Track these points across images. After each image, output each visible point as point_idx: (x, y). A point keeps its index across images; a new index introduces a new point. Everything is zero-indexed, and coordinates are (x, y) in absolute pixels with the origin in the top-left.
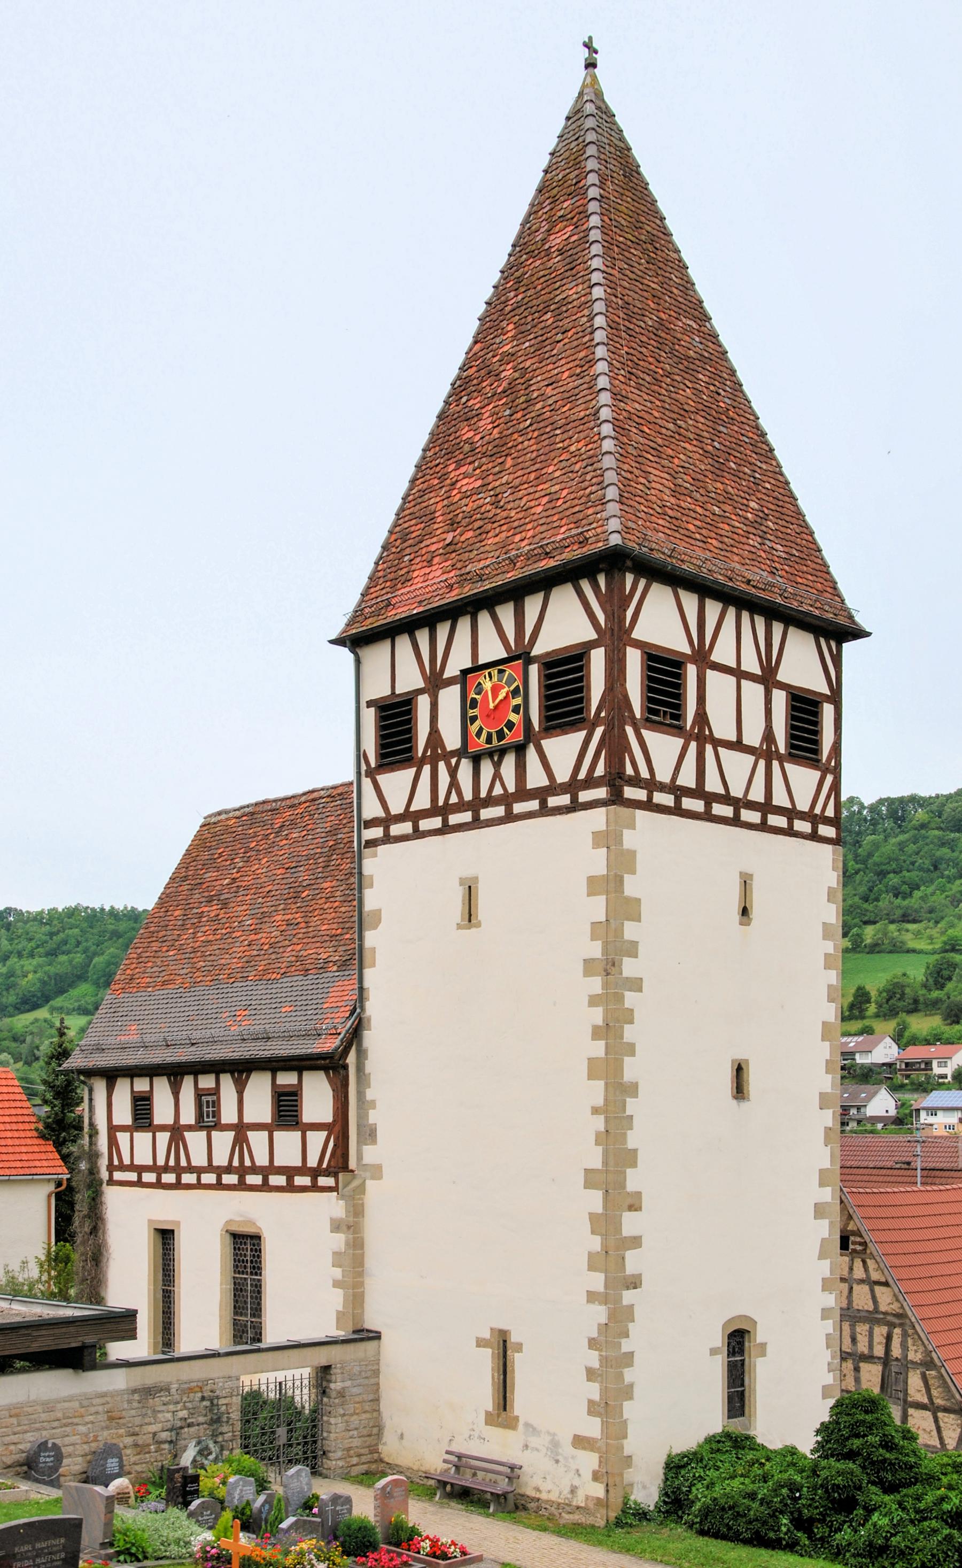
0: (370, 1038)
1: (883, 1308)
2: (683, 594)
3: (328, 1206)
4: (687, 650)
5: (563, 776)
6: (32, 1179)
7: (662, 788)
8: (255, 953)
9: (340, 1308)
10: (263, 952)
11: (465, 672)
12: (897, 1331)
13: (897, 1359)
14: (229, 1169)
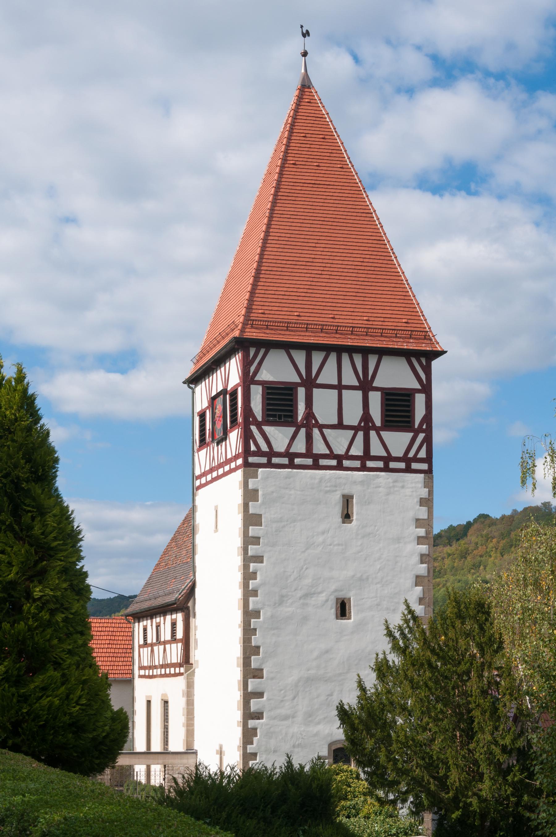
2: (294, 353)
4: (298, 380)
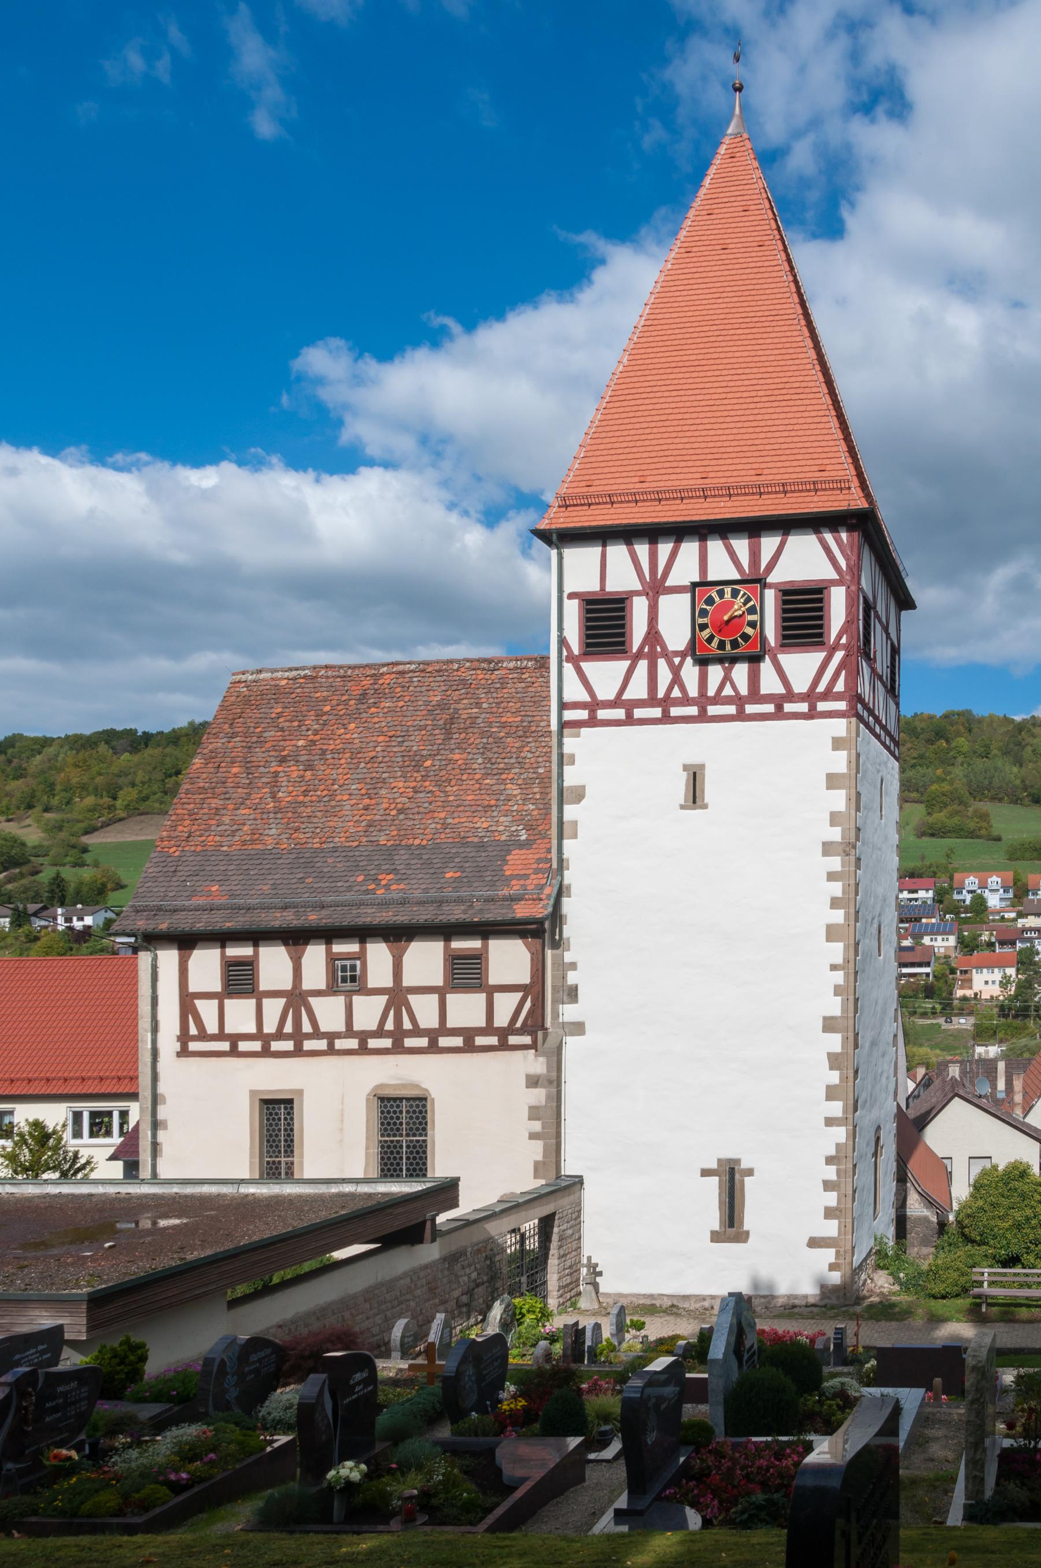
5: (800, 687)
9: (540, 1158)
11: (695, 585)
14: (279, 1035)
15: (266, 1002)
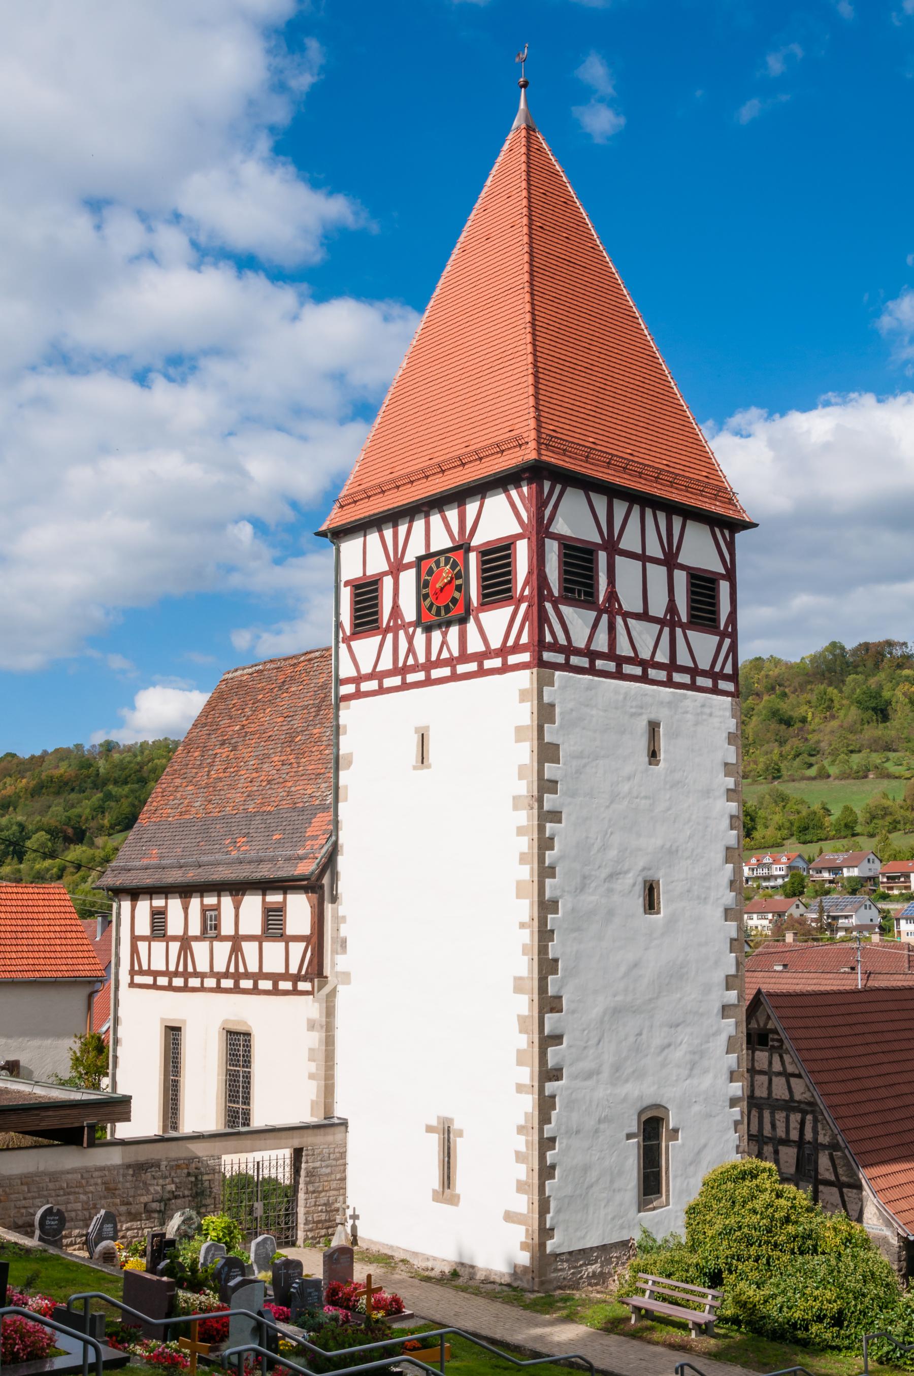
0: (342, 862)
1: (797, 1097)
3: (306, 1008)
5: (495, 644)
6: (76, 981)
7: (578, 652)
8: (255, 788)
10: (261, 788)
11: (420, 559)
12: (809, 1117)
13: (809, 1142)
14: (226, 975)
15: (292, 945)
